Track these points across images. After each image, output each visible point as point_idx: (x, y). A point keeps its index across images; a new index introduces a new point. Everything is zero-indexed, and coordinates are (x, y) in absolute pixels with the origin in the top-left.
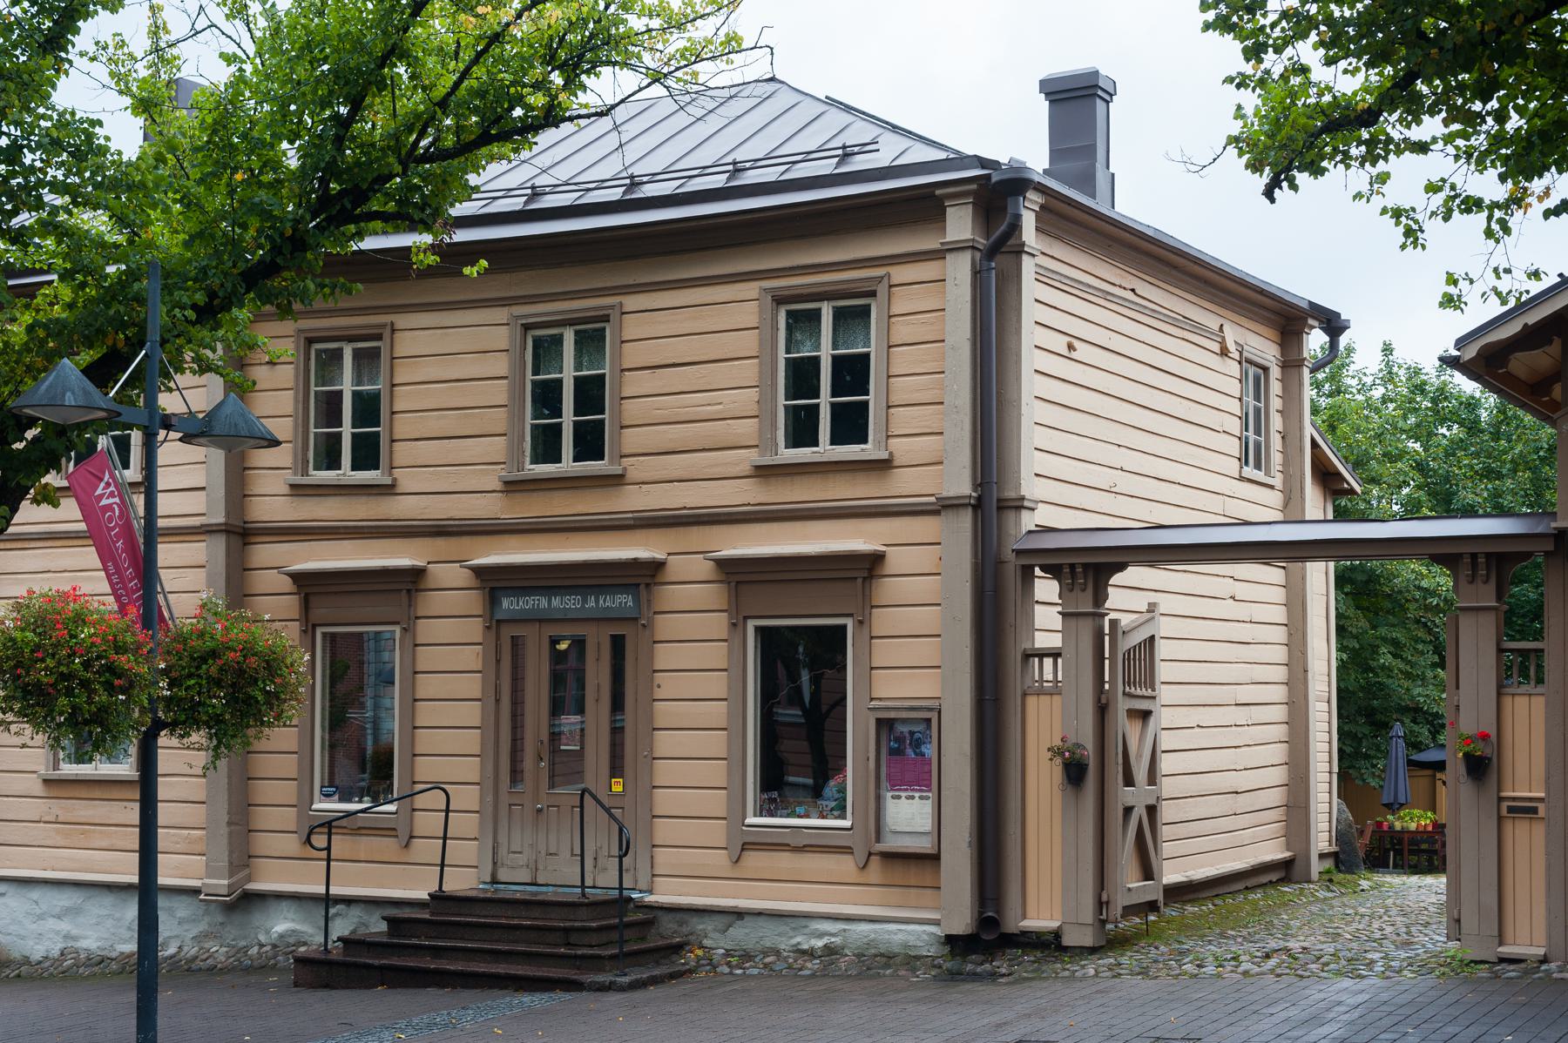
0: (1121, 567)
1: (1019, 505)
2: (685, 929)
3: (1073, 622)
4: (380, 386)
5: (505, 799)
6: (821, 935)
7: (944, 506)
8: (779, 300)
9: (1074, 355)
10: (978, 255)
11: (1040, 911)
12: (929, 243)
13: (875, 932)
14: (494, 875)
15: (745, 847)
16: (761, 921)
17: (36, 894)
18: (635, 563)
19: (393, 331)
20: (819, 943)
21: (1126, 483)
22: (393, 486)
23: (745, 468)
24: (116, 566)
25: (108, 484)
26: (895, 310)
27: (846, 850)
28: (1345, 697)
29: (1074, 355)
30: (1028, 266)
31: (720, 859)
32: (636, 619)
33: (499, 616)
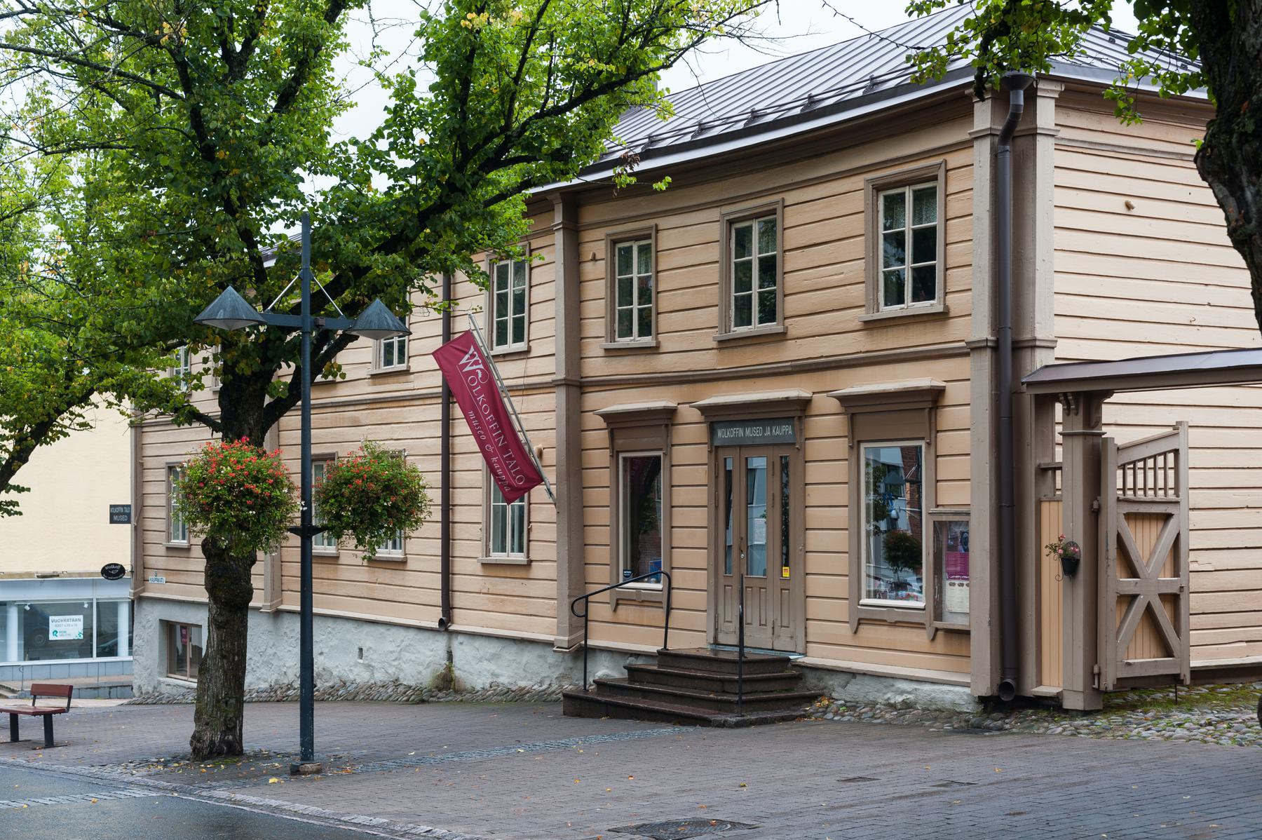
0: (1109, 393)
1: (1033, 346)
2: (822, 684)
3: (1069, 441)
5: (722, 582)
6: (902, 692)
7: (973, 349)
8: (878, 188)
9: (1133, 212)
10: (997, 139)
11: (1056, 672)
12: (960, 135)
13: (934, 691)
14: (716, 638)
15: (860, 622)
16: (866, 680)
17: (478, 643)
18: (787, 402)
19: (657, 231)
20: (899, 699)
21: (1203, 315)
22: (784, 334)
23: (857, 324)
24: (476, 413)
25: (473, 356)
26: (950, 190)
27: (920, 626)
29: (1133, 212)
30: (1044, 147)
31: (845, 630)
32: (794, 444)
33: (717, 443)
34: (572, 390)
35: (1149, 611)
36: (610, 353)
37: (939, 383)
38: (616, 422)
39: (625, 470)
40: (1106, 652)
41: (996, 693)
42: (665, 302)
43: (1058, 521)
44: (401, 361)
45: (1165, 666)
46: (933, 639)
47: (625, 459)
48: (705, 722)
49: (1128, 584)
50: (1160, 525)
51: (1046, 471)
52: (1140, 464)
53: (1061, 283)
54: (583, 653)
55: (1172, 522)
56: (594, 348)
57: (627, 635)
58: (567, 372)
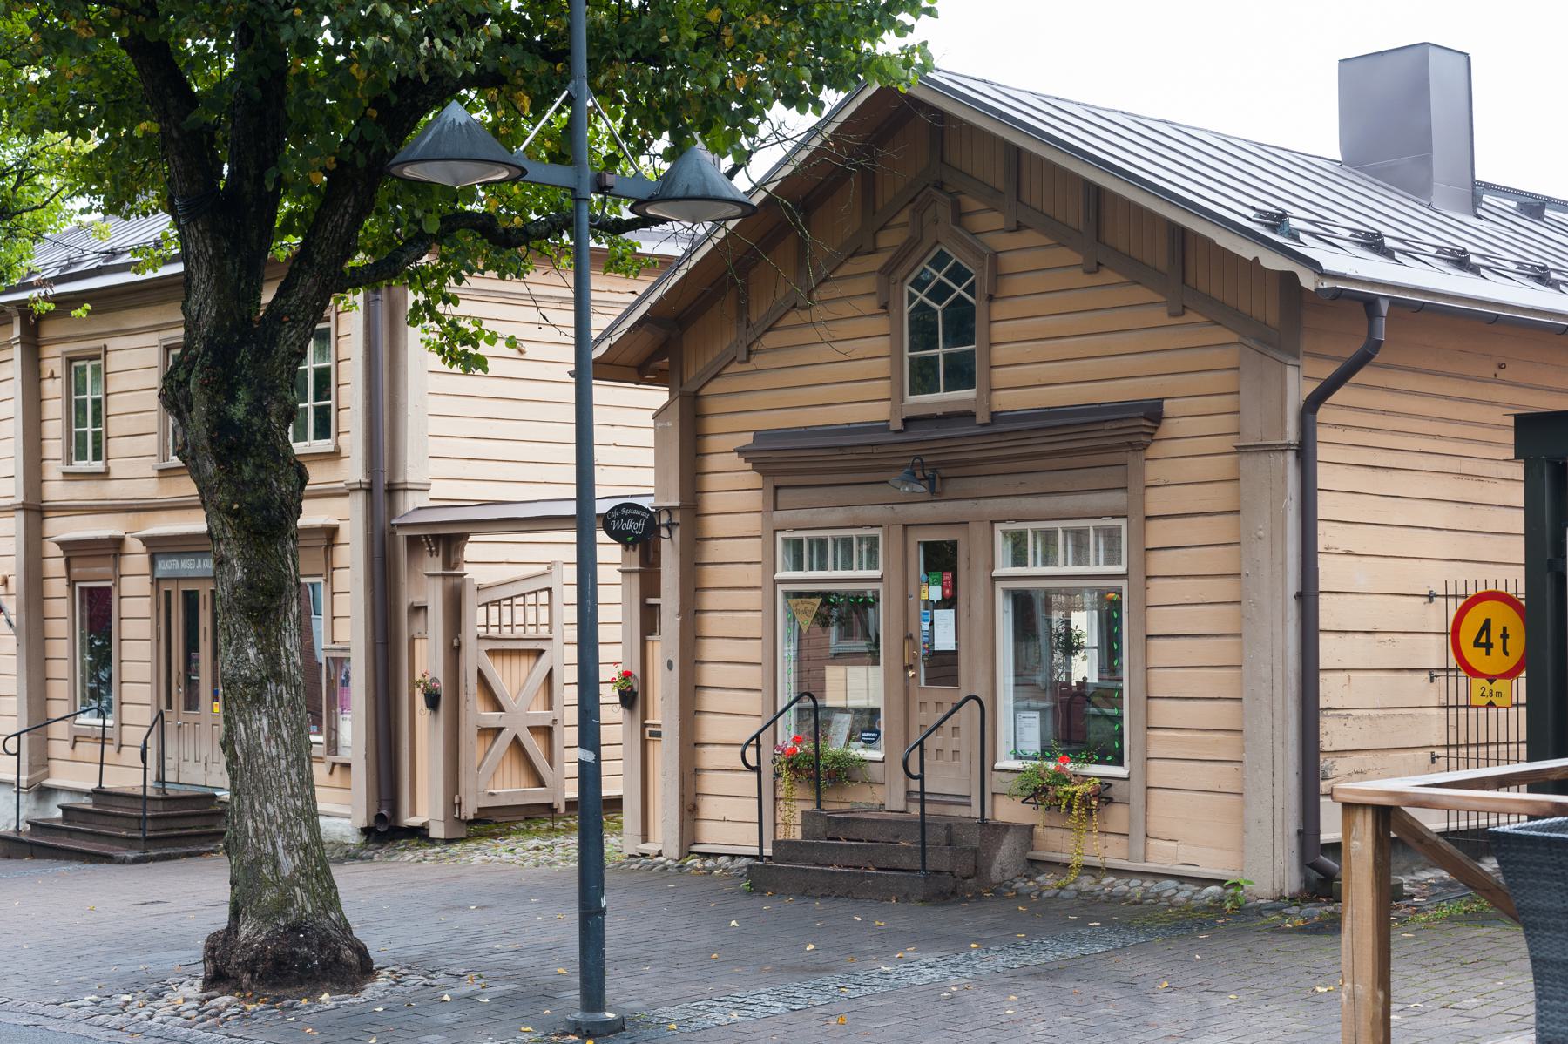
4: (331, 363)
7: (350, 491)
11: (425, 806)
28: (1033, 616)
34: (31, 514)
35: (516, 740)
36: (69, 476)
37: (333, 522)
38: (74, 550)
39: (82, 601)
40: (466, 783)
41: (372, 824)
42: (115, 426)
43: (426, 658)
44: (97, 456)
45: (536, 796)
46: (331, 773)
47: (82, 589)
48: (109, 859)
49: (492, 718)
50: (532, 660)
51: (418, 609)
52: (519, 600)
53: (435, 426)
54: (44, 793)
55: (544, 656)
56: (53, 469)
57: (74, 774)
58: (26, 495)
